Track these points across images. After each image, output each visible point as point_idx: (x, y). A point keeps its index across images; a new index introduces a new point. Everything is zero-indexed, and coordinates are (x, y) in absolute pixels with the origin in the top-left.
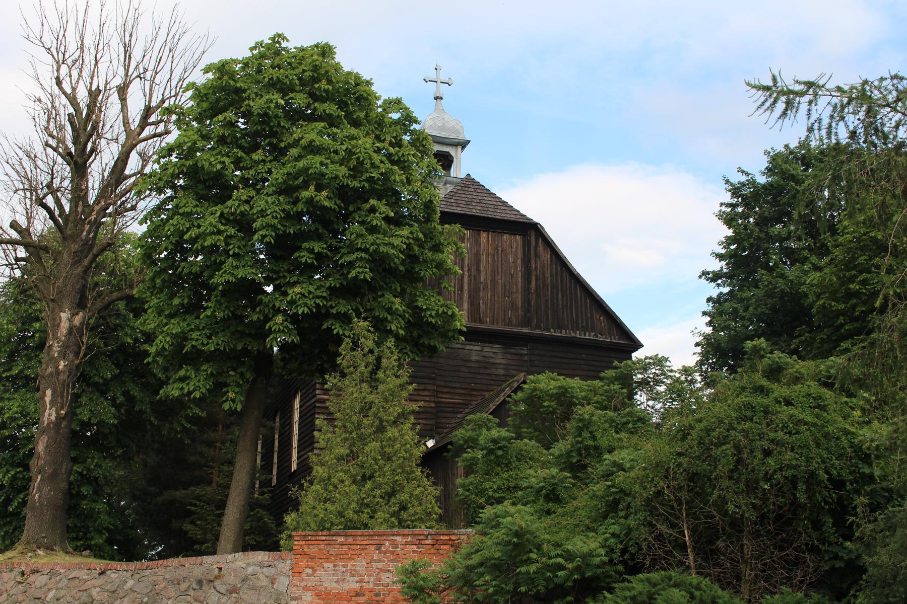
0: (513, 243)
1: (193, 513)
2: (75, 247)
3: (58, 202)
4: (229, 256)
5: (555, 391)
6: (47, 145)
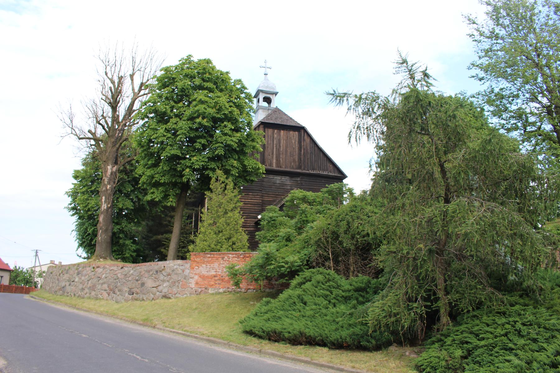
0: (294, 135)
1: (165, 245)
2: (113, 140)
3: (106, 122)
6: (102, 99)
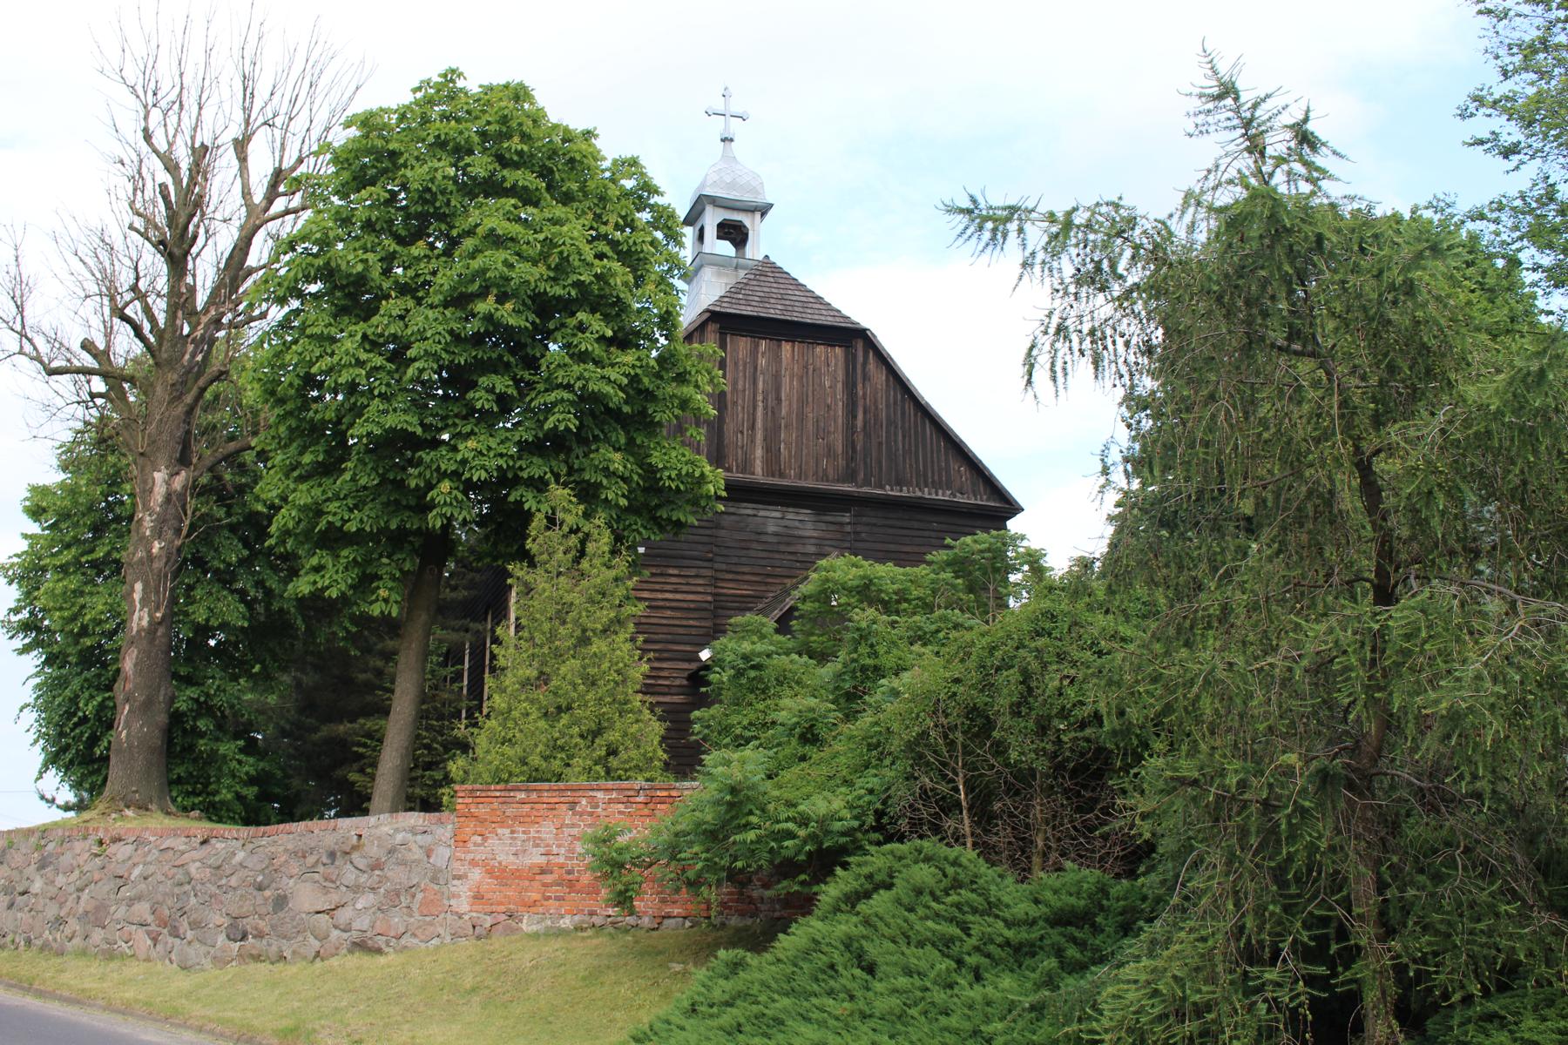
1: (361, 756)
2: (173, 377)
3: (148, 310)
4: (374, 397)
5: (855, 583)
6: (131, 227)
